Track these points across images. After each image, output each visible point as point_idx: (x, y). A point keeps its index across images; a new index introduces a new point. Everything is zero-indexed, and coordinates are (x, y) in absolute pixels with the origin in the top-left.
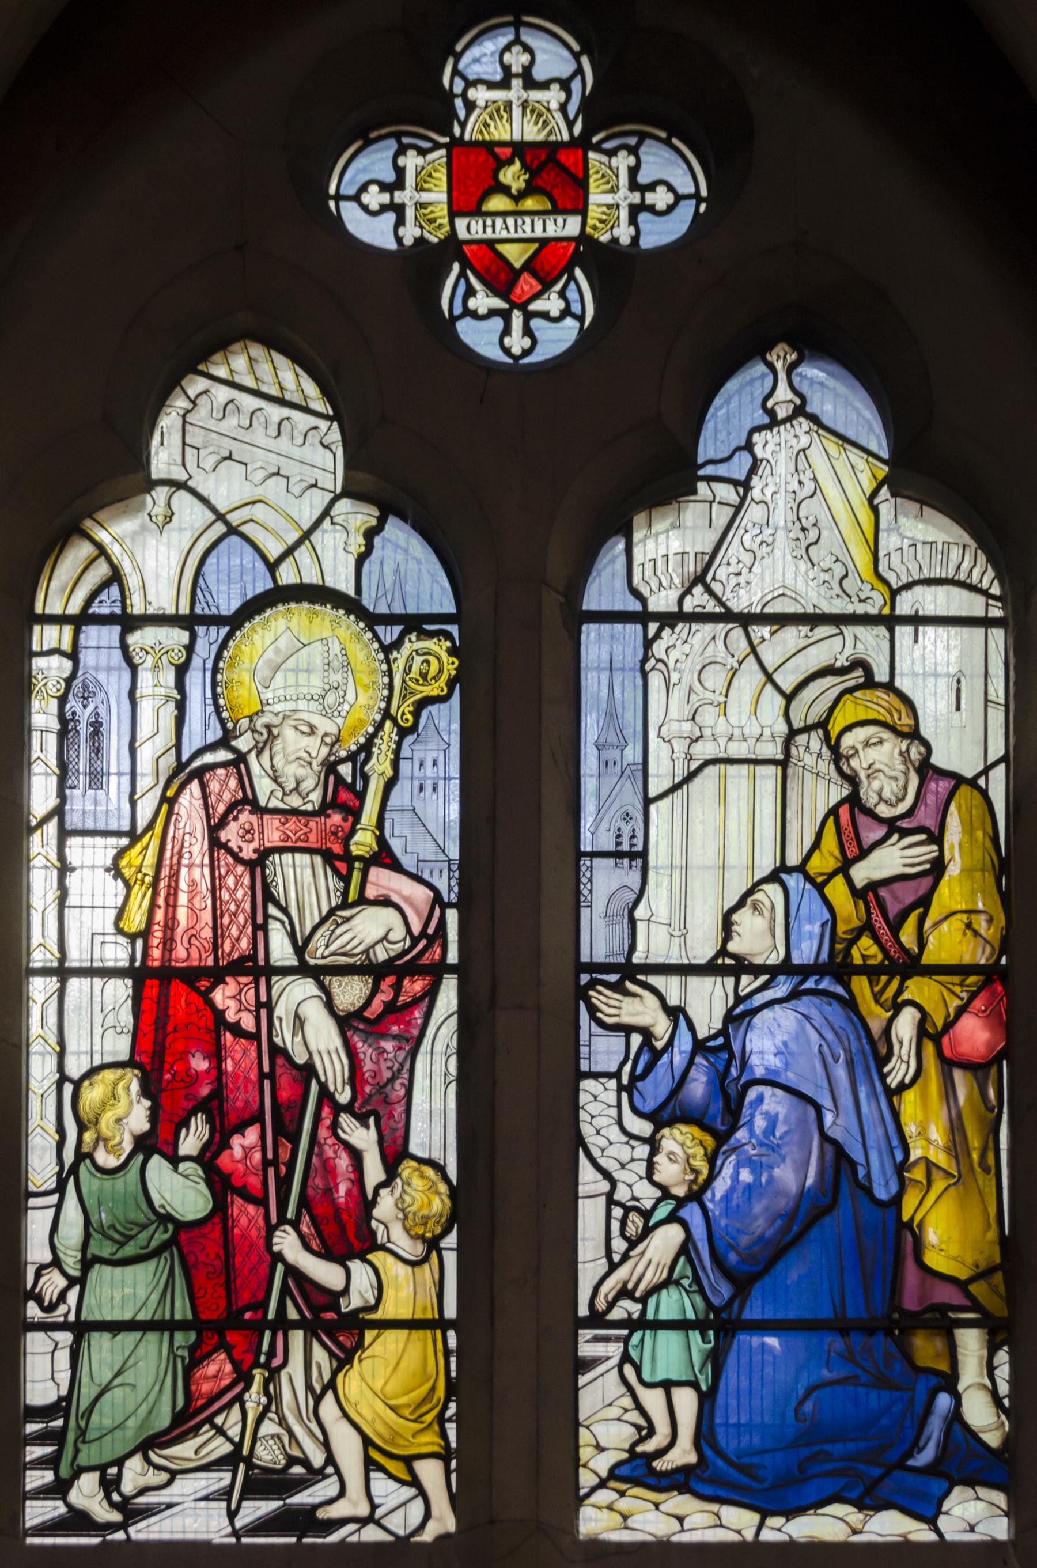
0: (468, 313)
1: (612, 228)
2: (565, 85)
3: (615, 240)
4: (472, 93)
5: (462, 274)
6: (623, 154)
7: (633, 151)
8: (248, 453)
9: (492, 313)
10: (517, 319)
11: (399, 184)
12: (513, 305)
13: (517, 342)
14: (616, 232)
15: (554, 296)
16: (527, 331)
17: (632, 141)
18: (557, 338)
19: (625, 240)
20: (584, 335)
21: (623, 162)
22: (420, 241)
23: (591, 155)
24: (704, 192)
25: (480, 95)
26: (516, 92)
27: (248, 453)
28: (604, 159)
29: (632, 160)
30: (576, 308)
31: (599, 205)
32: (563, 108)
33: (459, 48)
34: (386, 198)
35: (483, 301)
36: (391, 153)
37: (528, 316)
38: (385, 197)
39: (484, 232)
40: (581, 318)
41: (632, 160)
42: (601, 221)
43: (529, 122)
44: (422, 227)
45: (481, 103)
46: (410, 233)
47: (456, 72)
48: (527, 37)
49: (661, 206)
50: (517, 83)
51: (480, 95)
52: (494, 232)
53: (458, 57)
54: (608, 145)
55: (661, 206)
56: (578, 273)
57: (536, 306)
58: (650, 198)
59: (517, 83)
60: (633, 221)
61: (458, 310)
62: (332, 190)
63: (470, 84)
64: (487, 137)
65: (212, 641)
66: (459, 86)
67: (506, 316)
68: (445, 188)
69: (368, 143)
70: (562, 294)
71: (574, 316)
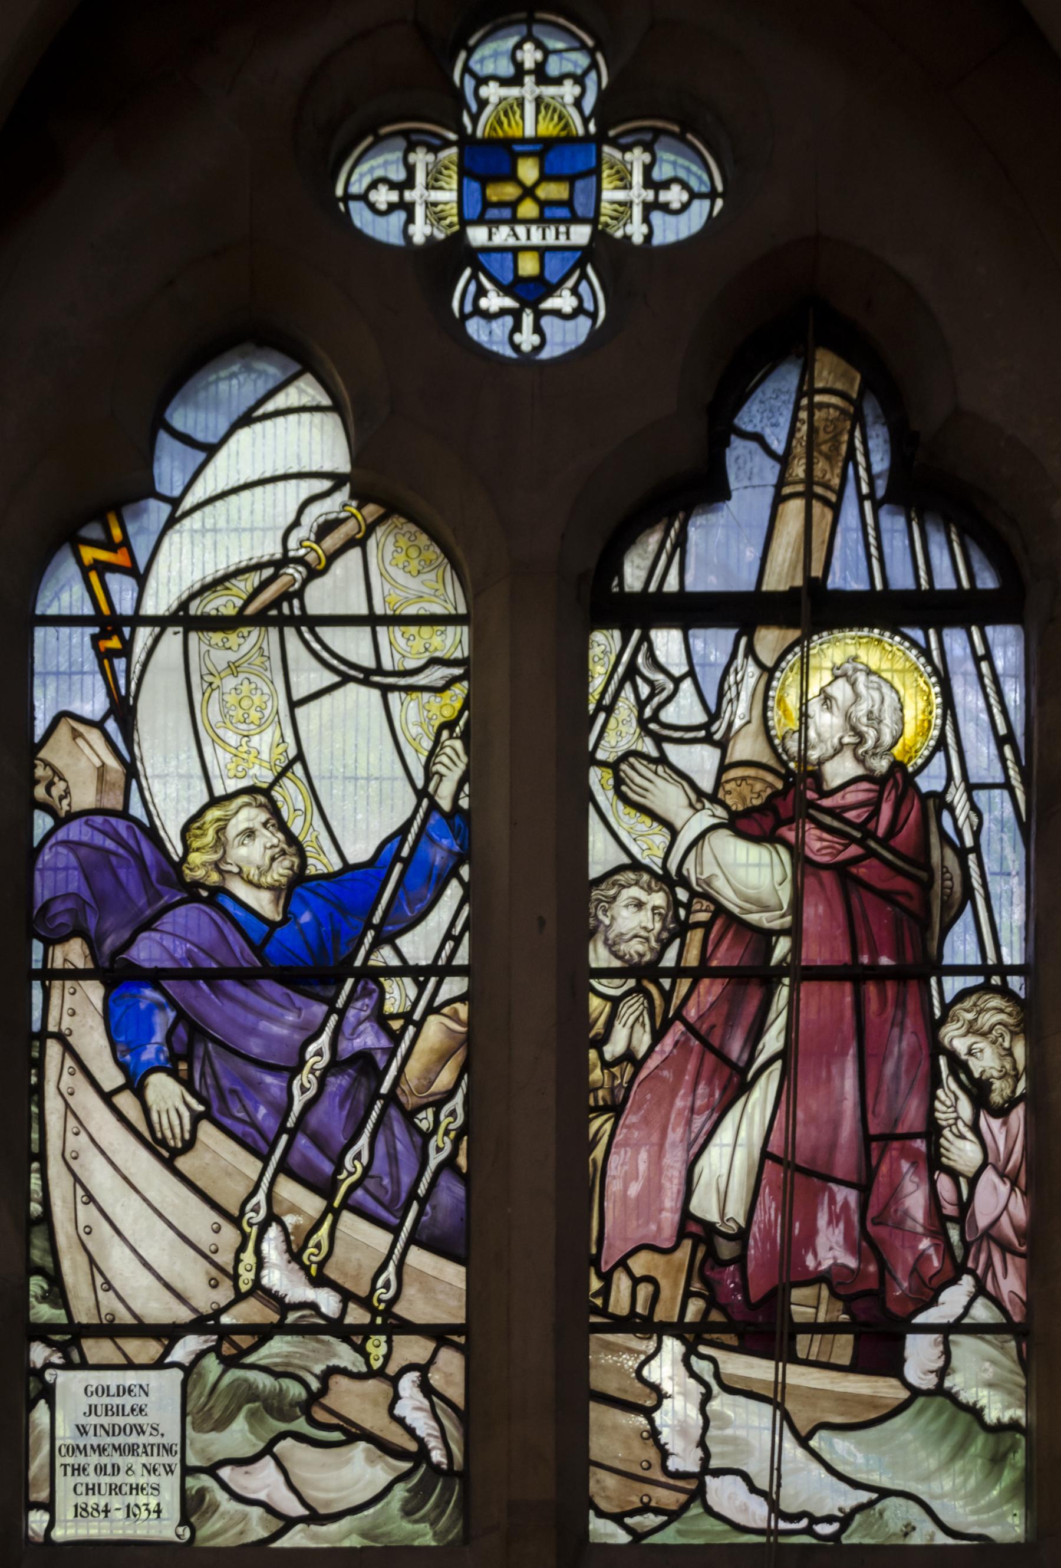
0: (478, 311)
1: (625, 225)
2: (579, 80)
3: (627, 238)
4: (484, 92)
5: (474, 276)
6: (637, 151)
7: (648, 147)
8: (261, 467)
9: (503, 312)
10: (528, 319)
11: (409, 183)
12: (524, 304)
13: (527, 339)
14: (629, 229)
15: (566, 293)
16: (538, 329)
17: (648, 137)
18: (565, 337)
19: (638, 240)
20: (593, 334)
21: (638, 158)
22: (430, 239)
23: (606, 149)
24: (720, 188)
25: (492, 92)
26: (530, 88)
27: (261, 467)
28: (618, 155)
29: (647, 158)
30: (589, 305)
31: (613, 202)
32: (578, 103)
33: (472, 42)
34: (394, 196)
35: (494, 301)
36: (399, 155)
37: (539, 314)
38: (399, 195)
39: (557, 238)
40: (593, 316)
41: (647, 158)
42: (612, 218)
43: (544, 118)
44: (432, 225)
45: (494, 100)
46: (420, 232)
47: (466, 69)
48: (537, 30)
49: (383, 189)
50: (528, 84)
51: (492, 92)
52: (568, 238)
53: (471, 51)
54: (623, 141)
55: (383, 189)
56: (590, 271)
57: (550, 304)
58: (664, 196)
59: (529, 80)
60: (646, 220)
61: (468, 308)
62: (339, 191)
63: (482, 81)
64: (500, 134)
65: (273, 1231)
66: (469, 84)
67: (516, 315)
68: (455, 186)
69: (379, 140)
70: (575, 291)
71: (587, 313)
